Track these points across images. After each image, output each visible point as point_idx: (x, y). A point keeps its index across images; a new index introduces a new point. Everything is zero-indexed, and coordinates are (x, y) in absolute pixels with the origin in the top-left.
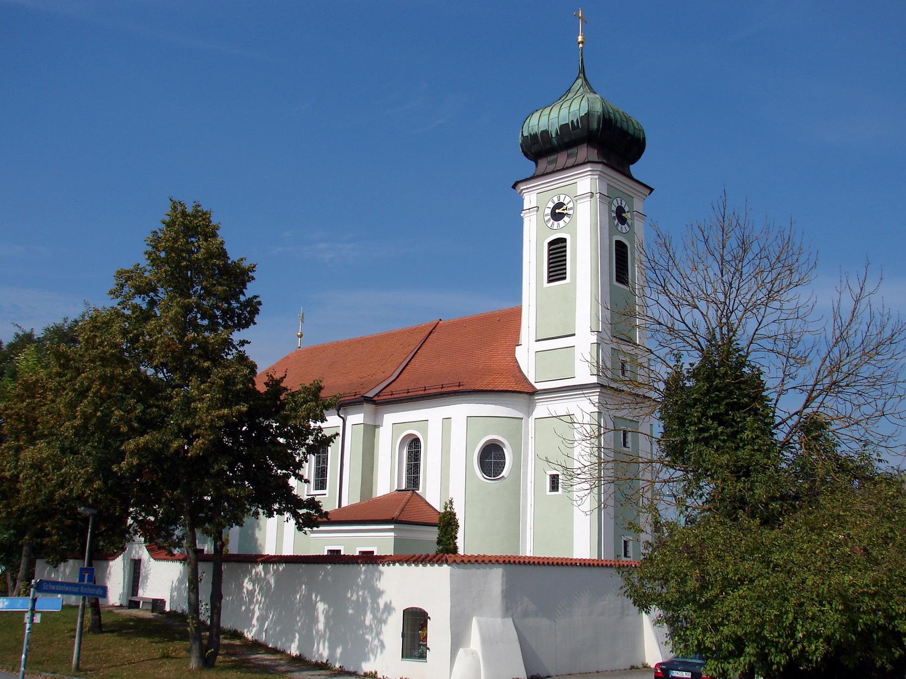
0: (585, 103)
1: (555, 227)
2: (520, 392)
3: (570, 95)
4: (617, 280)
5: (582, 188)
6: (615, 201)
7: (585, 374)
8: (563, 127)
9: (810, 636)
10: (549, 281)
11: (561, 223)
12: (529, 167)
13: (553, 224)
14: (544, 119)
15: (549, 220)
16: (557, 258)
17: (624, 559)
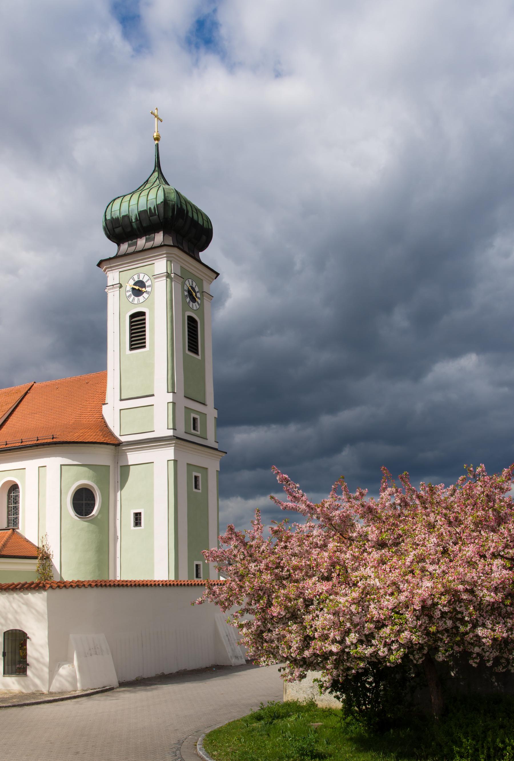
0: (161, 194)
1: (136, 302)
2: (107, 444)
3: (148, 186)
4: (189, 350)
5: (157, 270)
6: (187, 282)
7: (162, 427)
8: (140, 213)
9: (457, 653)
10: (131, 349)
11: (141, 298)
12: (111, 249)
13: (134, 299)
14: (125, 206)
15: (130, 296)
16: (138, 323)
17: (195, 579)
